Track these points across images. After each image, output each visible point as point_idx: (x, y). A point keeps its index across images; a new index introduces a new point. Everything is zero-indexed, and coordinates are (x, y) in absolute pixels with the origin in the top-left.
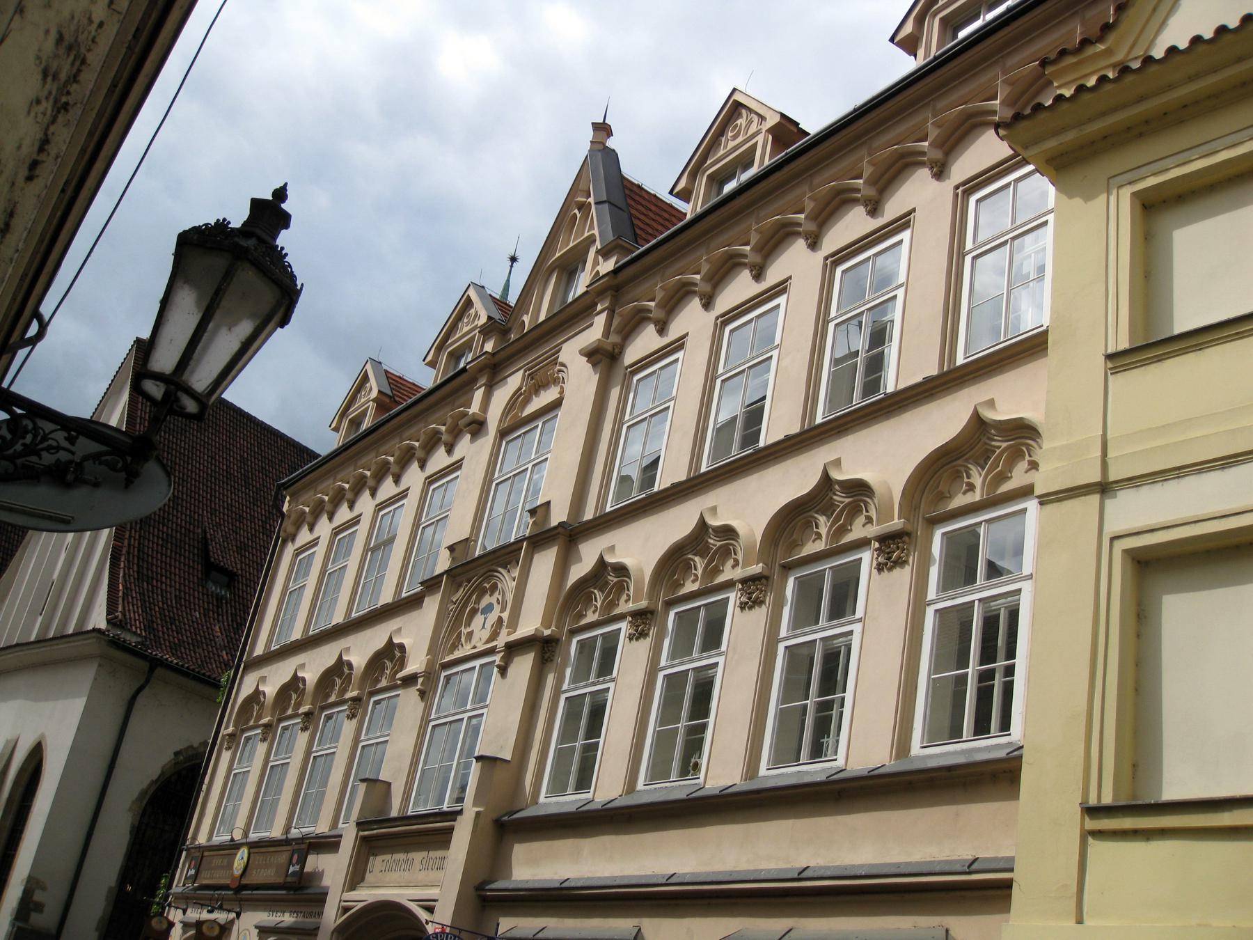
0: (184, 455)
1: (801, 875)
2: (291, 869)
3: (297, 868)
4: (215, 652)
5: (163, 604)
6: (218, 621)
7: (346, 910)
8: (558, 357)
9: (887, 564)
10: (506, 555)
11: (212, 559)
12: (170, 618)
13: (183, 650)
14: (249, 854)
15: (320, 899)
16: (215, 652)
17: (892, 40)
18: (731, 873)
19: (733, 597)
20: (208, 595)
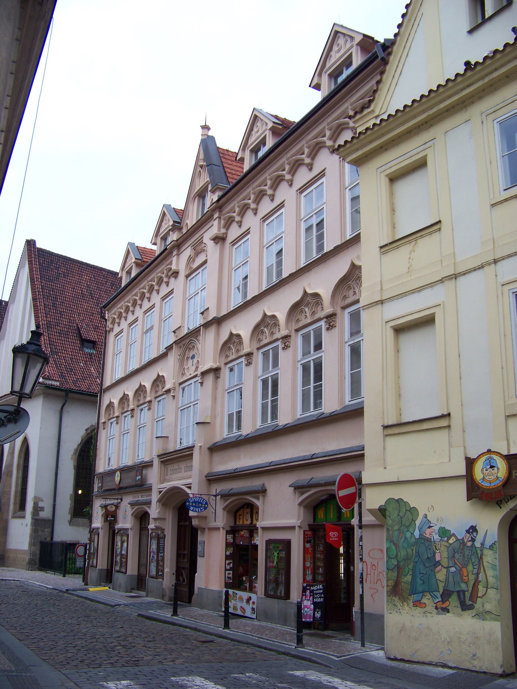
0: (60, 290)
1: (313, 457)
2: (138, 478)
3: (139, 477)
4: (94, 380)
5: (65, 363)
6: (92, 365)
7: (160, 492)
8: (203, 240)
10: (195, 333)
11: (83, 337)
12: (70, 369)
13: (79, 383)
14: (121, 474)
15: (150, 489)
16: (94, 380)
17: (310, 86)
18: (290, 459)
19: (322, 323)
20: (85, 354)
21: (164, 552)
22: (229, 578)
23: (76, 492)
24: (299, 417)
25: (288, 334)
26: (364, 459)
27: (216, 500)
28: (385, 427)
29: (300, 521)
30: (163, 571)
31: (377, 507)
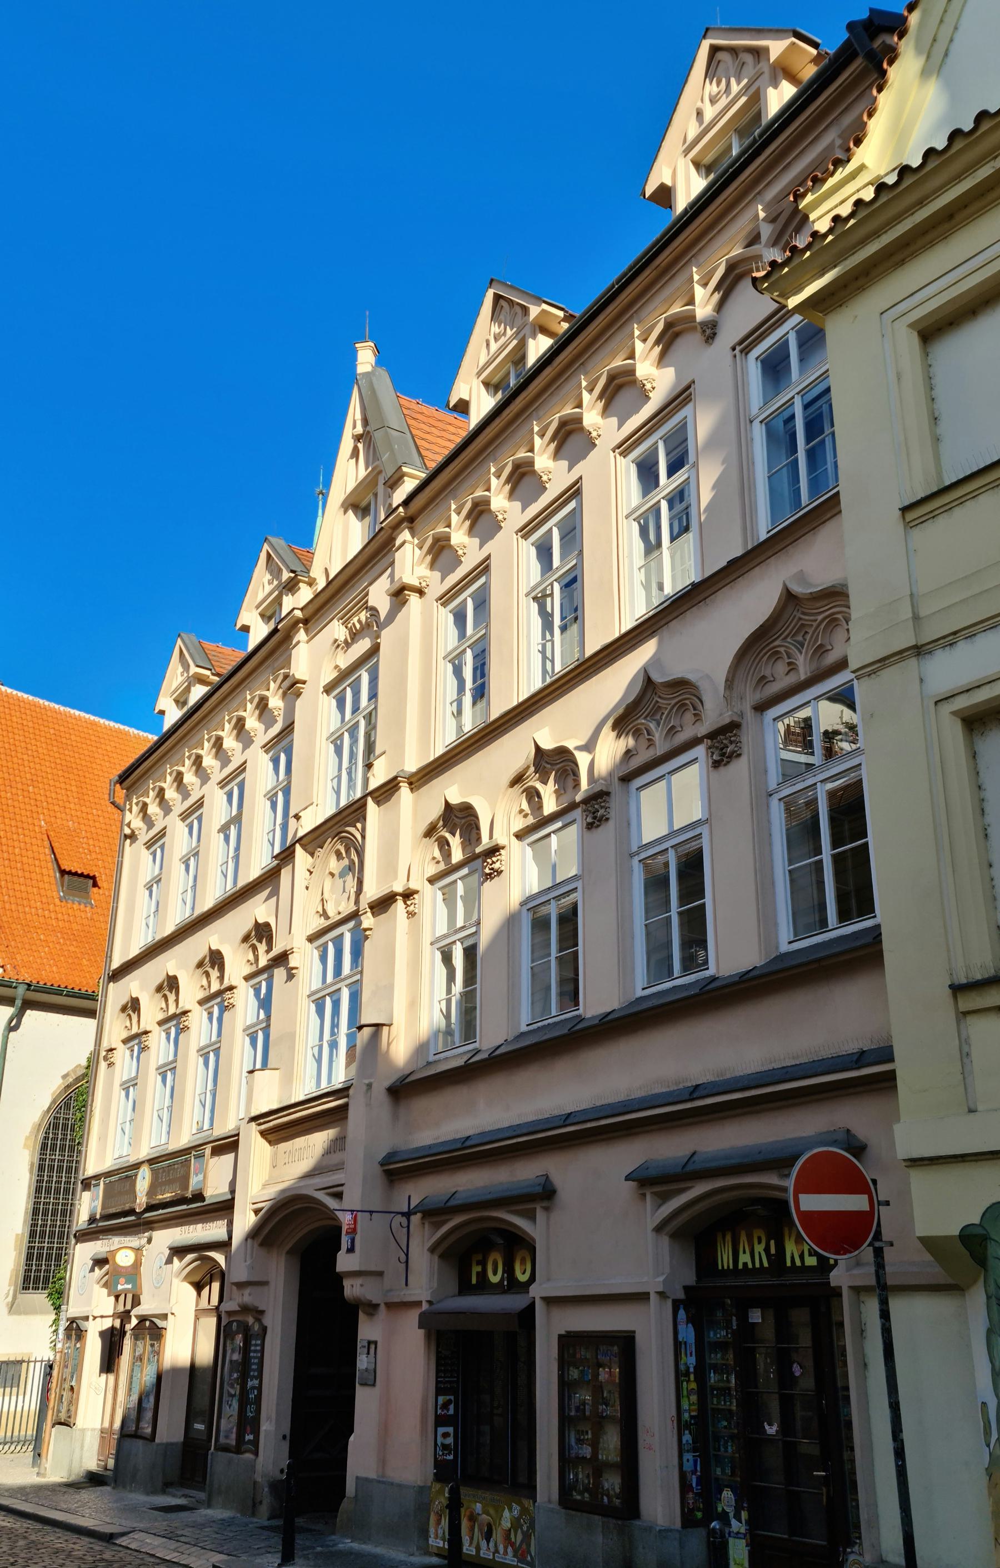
8: (367, 602)
9: (594, 823)
21: (260, 1377)
22: (445, 1447)
23: (709, 1540)
24: (640, 993)
25: (604, 789)
26: (895, 1087)
27: (408, 1227)
28: (957, 989)
29: (661, 1279)
30: (256, 1432)
31: (954, 1230)
